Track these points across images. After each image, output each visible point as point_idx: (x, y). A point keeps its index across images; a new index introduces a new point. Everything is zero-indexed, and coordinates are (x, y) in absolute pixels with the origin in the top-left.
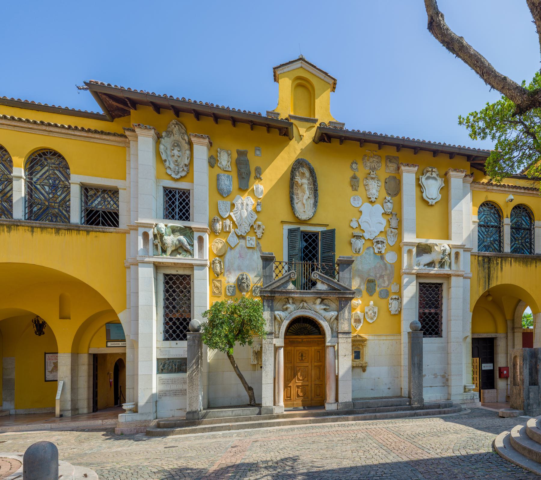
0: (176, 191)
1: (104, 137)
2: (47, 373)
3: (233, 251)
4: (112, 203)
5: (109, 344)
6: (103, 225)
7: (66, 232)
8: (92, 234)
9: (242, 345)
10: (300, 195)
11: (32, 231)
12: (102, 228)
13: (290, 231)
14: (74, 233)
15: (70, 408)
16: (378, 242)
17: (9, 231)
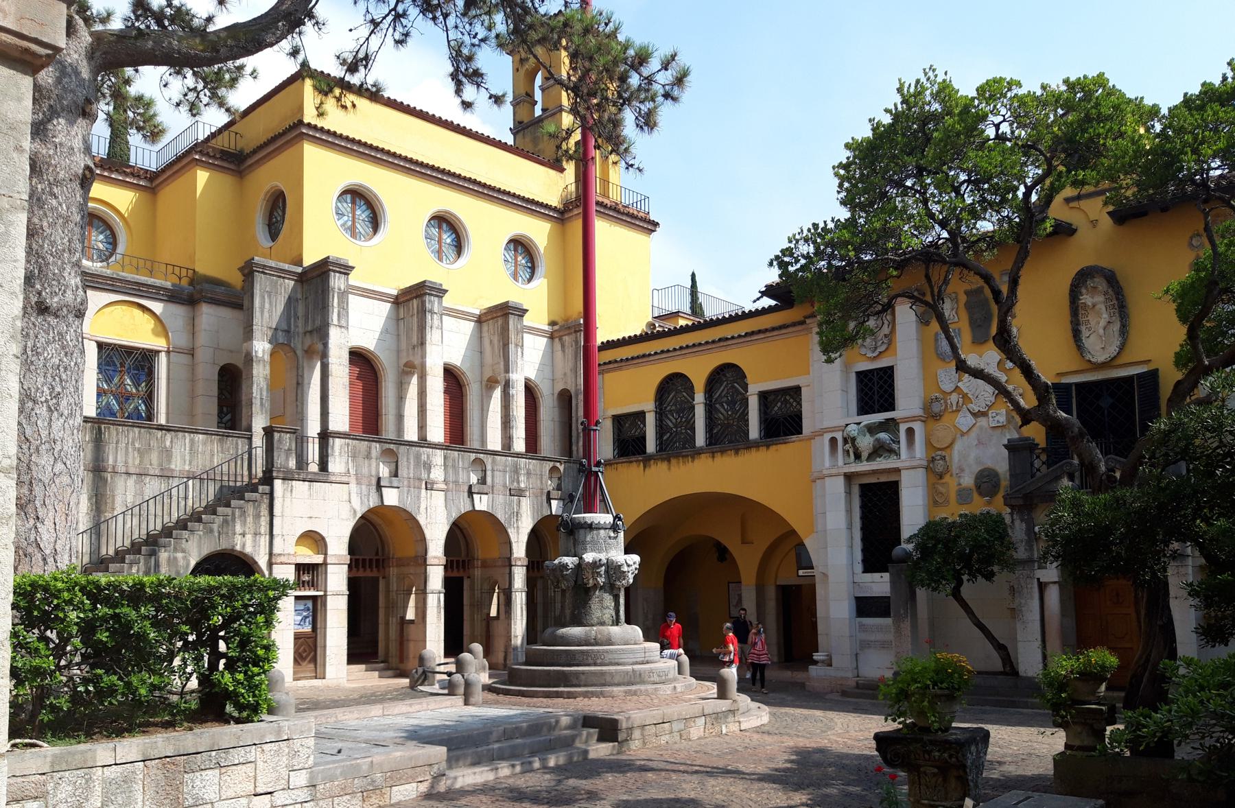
1: (784, 331)
2: (732, 608)
3: (965, 438)
4: (794, 404)
5: (801, 572)
8: (773, 448)
9: (971, 582)
10: (1093, 323)
11: (713, 457)
14: (754, 450)
15: (204, 316)
17: (693, 461)
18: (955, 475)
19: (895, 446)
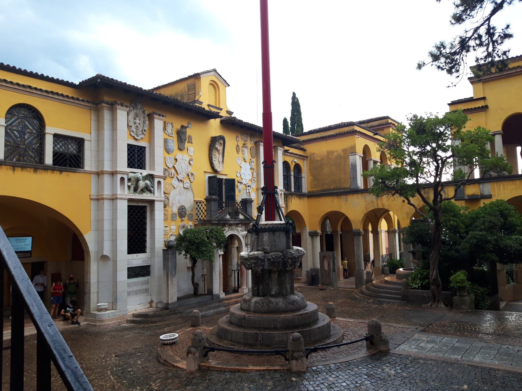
8: (65, 174)
11: (14, 170)
12: (74, 170)
13: (209, 178)
16: (248, 186)
18: (170, 207)
19: (152, 189)
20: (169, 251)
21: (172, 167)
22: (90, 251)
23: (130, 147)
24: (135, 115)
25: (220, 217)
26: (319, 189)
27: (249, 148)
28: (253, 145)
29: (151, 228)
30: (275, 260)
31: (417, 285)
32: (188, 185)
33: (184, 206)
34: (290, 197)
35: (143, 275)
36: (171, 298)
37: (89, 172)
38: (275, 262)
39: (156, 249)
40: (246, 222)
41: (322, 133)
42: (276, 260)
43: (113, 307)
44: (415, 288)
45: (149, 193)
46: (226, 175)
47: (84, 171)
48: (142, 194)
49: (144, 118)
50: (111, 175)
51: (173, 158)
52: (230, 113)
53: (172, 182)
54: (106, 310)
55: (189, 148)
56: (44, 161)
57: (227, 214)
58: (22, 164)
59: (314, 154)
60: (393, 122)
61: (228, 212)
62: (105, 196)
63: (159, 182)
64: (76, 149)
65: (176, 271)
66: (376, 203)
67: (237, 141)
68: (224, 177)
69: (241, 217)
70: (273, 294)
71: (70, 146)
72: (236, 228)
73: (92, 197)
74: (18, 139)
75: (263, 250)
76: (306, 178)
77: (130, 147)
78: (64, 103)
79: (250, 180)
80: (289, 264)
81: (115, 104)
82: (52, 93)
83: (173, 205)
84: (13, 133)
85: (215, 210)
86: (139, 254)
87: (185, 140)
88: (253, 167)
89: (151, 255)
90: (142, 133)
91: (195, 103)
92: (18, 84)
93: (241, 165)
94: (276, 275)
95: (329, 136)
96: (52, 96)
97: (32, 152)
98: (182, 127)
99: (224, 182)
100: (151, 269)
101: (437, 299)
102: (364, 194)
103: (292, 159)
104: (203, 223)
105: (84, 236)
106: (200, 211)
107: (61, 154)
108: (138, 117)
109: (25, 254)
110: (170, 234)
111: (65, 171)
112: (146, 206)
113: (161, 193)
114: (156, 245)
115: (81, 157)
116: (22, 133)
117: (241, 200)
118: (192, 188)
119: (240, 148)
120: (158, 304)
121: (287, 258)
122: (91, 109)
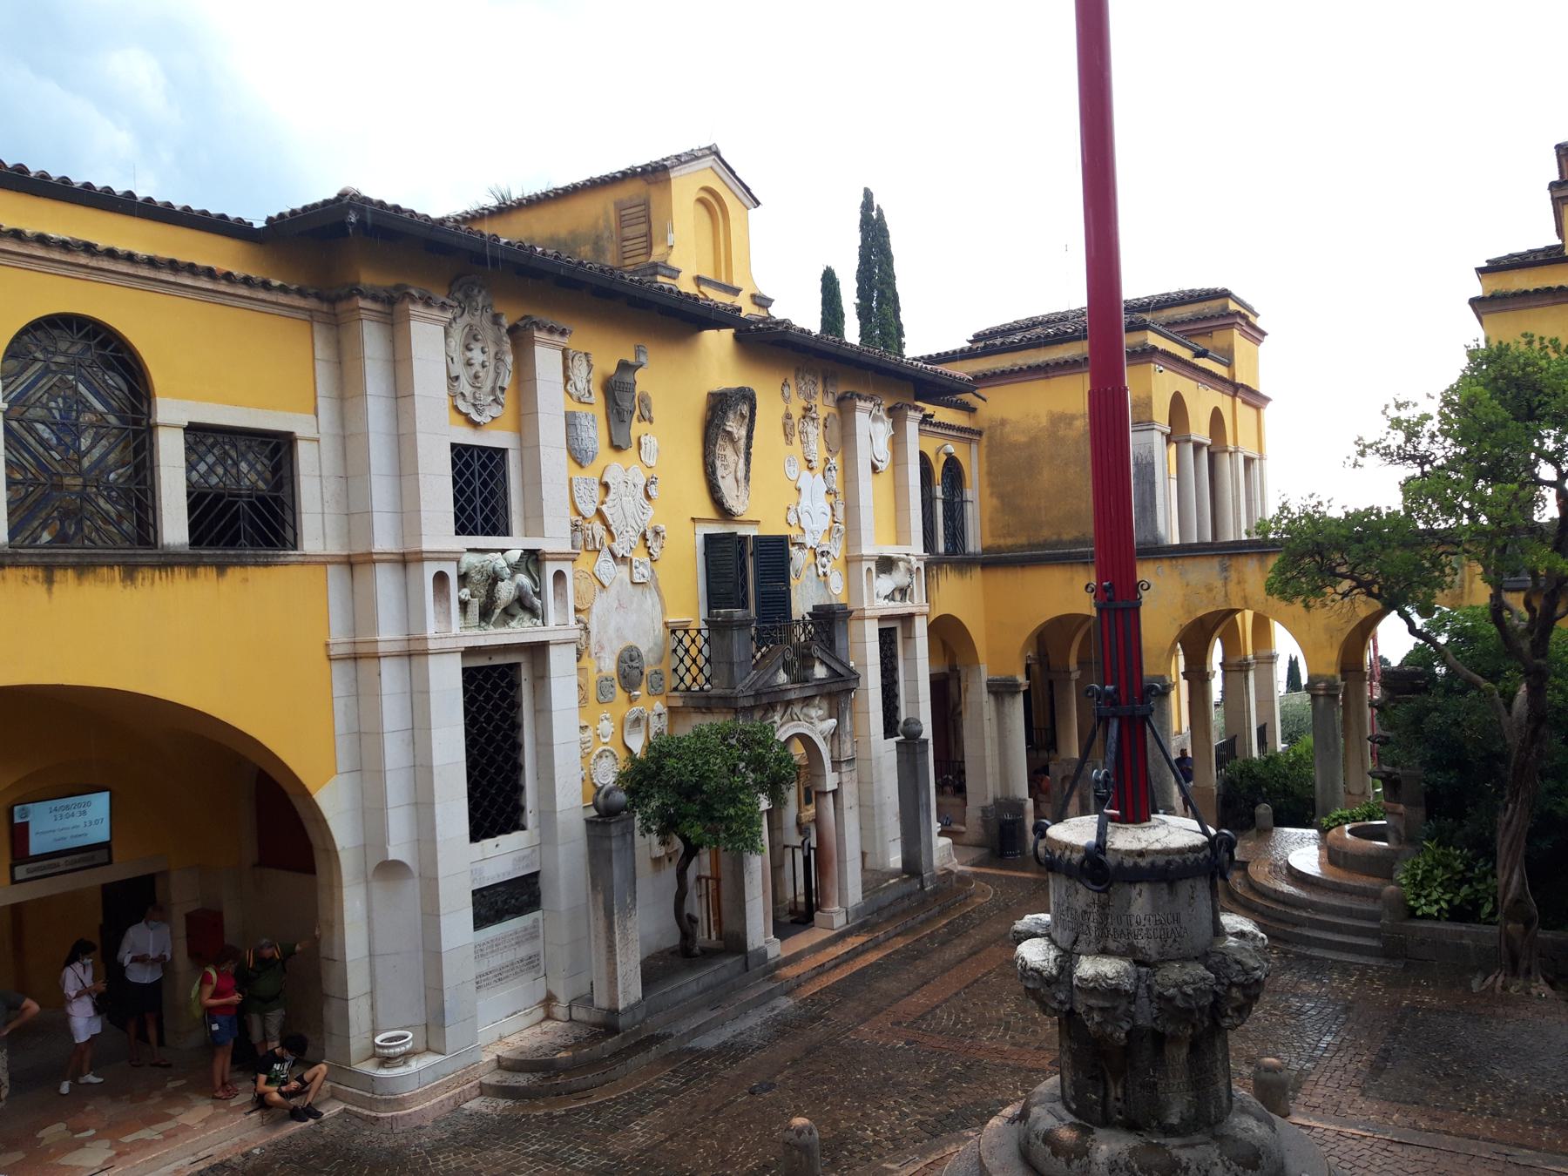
0: (472, 453)
6: (253, 544)
7: (157, 573)
8: (234, 574)
11: (50, 581)
12: (267, 556)
14: (181, 575)
16: (823, 554)
19: (537, 602)
20: (613, 828)
21: (593, 513)
22: (339, 848)
23: (459, 451)
24: (468, 334)
25: (761, 682)
26: (1023, 540)
27: (821, 421)
28: (833, 410)
29: (537, 739)
30: (1193, 1002)
31: (1436, 907)
32: (646, 574)
33: (636, 648)
34: (935, 572)
35: (519, 911)
36: (625, 992)
37: (318, 559)
38: (1190, 1011)
39: (558, 815)
40: (835, 687)
41: (1032, 352)
42: (1196, 1003)
43: (427, 1042)
44: (1426, 917)
45: (526, 617)
46: (757, 522)
47: (300, 559)
48: (505, 623)
49: (498, 342)
50: (400, 567)
51: (597, 481)
52: (762, 301)
53: (596, 567)
54: (406, 1056)
55: (642, 440)
56: (156, 532)
57: (779, 669)
58: (78, 555)
59: (1003, 422)
60: (1243, 311)
61: (781, 662)
62: (382, 648)
63: (559, 576)
64: (268, 475)
65: (635, 892)
66: (1223, 593)
67: (786, 399)
68: (751, 531)
69: (820, 672)
70: (1172, 1125)
71: (244, 466)
72: (805, 710)
73: (336, 651)
74: (53, 453)
75: (1129, 952)
76: (977, 503)
77: (459, 451)
78: (217, 300)
79: (827, 532)
80: (1233, 1005)
81: (404, 298)
82: (173, 266)
83: (602, 648)
84: (31, 430)
85: (742, 659)
86: (501, 839)
87: (632, 413)
88: (834, 486)
89: (541, 835)
90: (492, 398)
91: (656, 273)
92: (42, 240)
93: (798, 485)
94: (1185, 1050)
95: (1057, 364)
96: (172, 279)
97: (108, 499)
98: (624, 367)
99: (750, 547)
100: (543, 884)
101: (1523, 964)
102: (1180, 561)
103: (938, 442)
104: (703, 703)
105: (314, 796)
106: (688, 661)
107: (218, 497)
108: (477, 340)
109: (90, 854)
110: (597, 752)
111: (235, 565)
112: (517, 665)
113: (567, 614)
114: (559, 799)
115: (288, 501)
116: (68, 428)
117: (811, 610)
118: (657, 579)
119: (796, 421)
120: (574, 1009)
121: (1226, 981)
122: (311, 317)
